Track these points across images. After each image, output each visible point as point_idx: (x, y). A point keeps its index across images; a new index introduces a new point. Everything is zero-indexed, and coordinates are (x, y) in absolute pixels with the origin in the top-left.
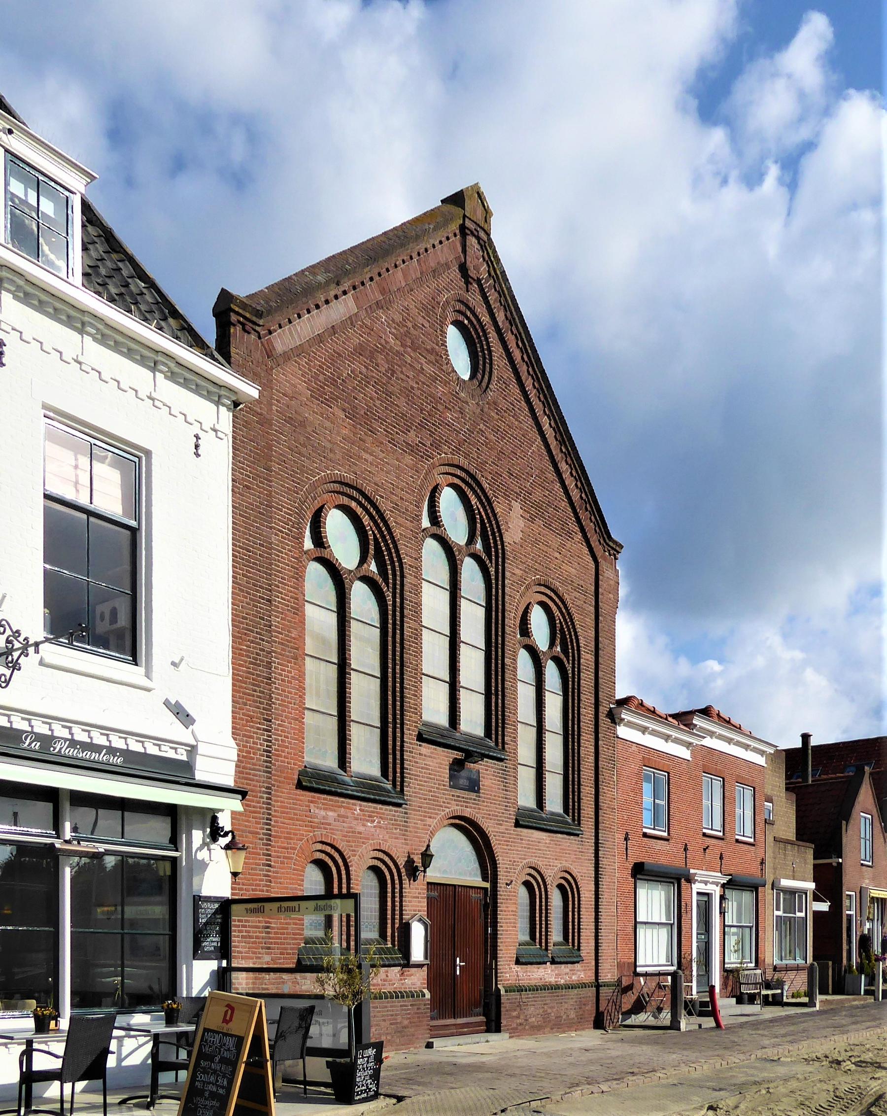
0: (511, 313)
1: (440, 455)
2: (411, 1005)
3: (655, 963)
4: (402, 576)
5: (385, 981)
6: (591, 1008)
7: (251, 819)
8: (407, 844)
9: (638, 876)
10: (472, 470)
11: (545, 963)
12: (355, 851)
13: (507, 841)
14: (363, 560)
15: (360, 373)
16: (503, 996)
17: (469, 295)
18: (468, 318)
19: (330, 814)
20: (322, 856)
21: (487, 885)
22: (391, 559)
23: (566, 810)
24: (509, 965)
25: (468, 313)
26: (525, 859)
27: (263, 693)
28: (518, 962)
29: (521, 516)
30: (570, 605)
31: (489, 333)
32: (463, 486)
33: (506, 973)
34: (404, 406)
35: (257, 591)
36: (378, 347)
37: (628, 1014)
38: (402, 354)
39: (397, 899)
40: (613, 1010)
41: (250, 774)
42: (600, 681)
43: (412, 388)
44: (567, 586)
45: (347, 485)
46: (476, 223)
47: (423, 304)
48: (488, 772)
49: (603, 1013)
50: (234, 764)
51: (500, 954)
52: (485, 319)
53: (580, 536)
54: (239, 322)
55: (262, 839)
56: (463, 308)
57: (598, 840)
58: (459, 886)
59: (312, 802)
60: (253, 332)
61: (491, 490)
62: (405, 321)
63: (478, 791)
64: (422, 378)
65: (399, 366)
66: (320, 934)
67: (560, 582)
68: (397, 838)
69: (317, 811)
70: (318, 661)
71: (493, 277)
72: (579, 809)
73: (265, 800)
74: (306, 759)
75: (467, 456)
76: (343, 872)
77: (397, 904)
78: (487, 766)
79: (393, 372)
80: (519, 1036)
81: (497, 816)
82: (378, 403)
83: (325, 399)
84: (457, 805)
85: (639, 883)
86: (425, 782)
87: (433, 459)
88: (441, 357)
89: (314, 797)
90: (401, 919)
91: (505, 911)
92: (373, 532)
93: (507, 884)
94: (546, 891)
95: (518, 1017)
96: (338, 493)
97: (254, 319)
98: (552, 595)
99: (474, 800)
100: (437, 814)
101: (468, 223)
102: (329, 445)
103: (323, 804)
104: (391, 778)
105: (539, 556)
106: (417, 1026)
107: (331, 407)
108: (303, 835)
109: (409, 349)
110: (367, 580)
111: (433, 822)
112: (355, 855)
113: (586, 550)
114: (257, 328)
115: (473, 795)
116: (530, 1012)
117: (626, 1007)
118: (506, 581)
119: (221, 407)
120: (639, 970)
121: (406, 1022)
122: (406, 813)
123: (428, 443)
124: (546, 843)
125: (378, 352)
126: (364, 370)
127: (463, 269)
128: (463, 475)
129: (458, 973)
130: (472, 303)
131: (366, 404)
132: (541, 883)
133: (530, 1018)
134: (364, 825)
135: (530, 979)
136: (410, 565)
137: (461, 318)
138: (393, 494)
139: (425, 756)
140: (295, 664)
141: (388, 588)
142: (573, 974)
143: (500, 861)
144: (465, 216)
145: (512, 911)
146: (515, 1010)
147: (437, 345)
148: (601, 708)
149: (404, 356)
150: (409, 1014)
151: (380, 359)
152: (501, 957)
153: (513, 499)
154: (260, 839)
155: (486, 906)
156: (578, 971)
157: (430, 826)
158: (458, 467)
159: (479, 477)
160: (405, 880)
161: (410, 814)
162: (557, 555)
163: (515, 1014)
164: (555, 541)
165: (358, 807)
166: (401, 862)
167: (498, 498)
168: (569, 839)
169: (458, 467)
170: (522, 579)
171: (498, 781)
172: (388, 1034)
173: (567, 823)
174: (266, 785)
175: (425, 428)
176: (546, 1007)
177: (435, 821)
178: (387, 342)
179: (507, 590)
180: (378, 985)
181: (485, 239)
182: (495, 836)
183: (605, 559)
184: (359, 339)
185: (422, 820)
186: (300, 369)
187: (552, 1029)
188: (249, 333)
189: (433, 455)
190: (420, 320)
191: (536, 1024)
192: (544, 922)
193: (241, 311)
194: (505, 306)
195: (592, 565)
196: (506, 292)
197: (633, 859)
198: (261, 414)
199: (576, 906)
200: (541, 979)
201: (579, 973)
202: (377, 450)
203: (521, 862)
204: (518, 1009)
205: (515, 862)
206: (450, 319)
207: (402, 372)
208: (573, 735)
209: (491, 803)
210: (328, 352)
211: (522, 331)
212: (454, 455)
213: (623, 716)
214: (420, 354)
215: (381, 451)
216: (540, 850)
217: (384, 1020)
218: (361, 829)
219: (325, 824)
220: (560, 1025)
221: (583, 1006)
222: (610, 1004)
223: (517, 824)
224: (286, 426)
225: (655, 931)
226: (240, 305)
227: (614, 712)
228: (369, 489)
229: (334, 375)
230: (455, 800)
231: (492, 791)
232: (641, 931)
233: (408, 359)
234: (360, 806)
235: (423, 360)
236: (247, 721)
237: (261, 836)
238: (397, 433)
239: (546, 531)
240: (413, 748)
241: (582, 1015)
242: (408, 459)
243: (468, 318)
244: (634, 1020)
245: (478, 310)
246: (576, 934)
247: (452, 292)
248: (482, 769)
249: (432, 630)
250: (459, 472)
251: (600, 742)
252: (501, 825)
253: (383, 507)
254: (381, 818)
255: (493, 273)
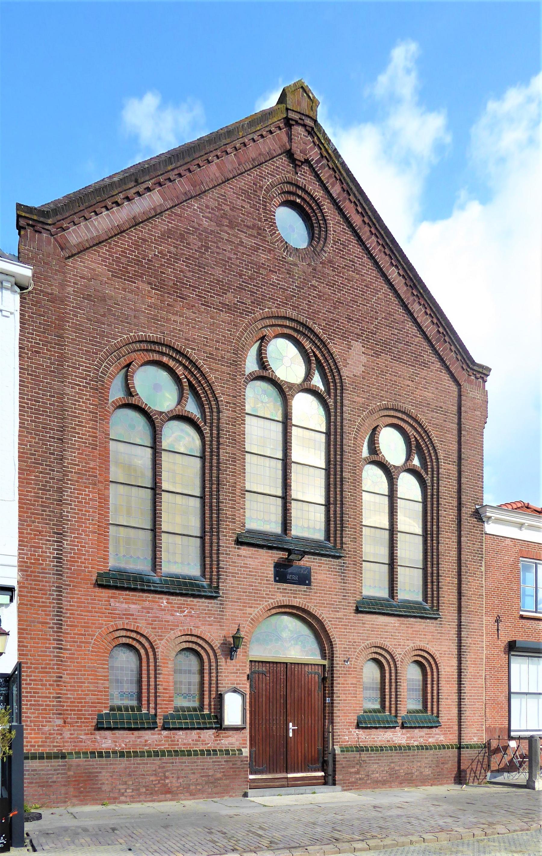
0: (347, 184)
1: (263, 310)
2: (225, 761)
3: (524, 728)
4: (219, 412)
5: (197, 741)
6: (452, 765)
7: (40, 612)
8: (223, 630)
9: (512, 653)
10: (302, 319)
11: (394, 727)
12: (161, 636)
13: (345, 625)
14: (409, 457)
15: (168, 252)
16: (339, 755)
17: (298, 177)
18: (299, 197)
19: (133, 606)
20: (185, 645)
21: (325, 662)
22: (208, 399)
23: (425, 599)
24: (349, 729)
25: (300, 192)
26: (367, 640)
27: (53, 512)
28: (358, 727)
29: (363, 353)
30: (425, 424)
31: (323, 205)
32: (295, 335)
33: (344, 736)
34: (221, 274)
35: (46, 432)
36: (189, 229)
37: (500, 771)
38: (218, 233)
39: (214, 675)
40: (479, 768)
41: (39, 577)
42: (463, 486)
43: (230, 258)
44: (421, 408)
45: (154, 343)
46: (300, 113)
47: (243, 190)
48: (322, 568)
49: (465, 771)
50: (16, 569)
51: (336, 720)
52: (319, 194)
53: (438, 365)
54: (28, 225)
55: (53, 628)
56: (292, 189)
57: (461, 622)
58: (291, 663)
59: (112, 597)
60: (43, 231)
61: (326, 334)
62: (221, 205)
63: (309, 584)
64: (241, 249)
65: (214, 242)
66: (134, 703)
67: (412, 405)
68: (211, 625)
69: (117, 604)
70: (130, 487)
71: (326, 157)
72: (438, 597)
73: (55, 597)
74: (363, 594)
75: (294, 308)
76: (435, 670)
77: (214, 678)
78: (320, 563)
79: (207, 248)
80: (358, 789)
81: (333, 604)
82: (189, 274)
83: (128, 277)
84: (283, 596)
85: (513, 659)
86: (244, 578)
87: (254, 314)
88: (264, 230)
89: (114, 594)
90: (217, 691)
91: (343, 684)
92: (188, 380)
93: (344, 661)
94: (396, 667)
95: (358, 773)
96: (147, 350)
97: (42, 219)
98: (405, 417)
99: (304, 591)
100: (260, 604)
101: (291, 115)
102: (132, 313)
103: (124, 599)
104: (208, 577)
105: (386, 385)
106: (233, 778)
107: (135, 283)
108: (102, 624)
109: (226, 228)
110: (413, 471)
111: (254, 612)
112: (162, 640)
113: (447, 377)
114: (47, 227)
115: (303, 588)
116: (373, 769)
117: (494, 767)
118: (345, 409)
119: (4, 291)
120: (513, 734)
121: (219, 775)
122: (221, 604)
123: (249, 302)
124: (395, 626)
125: (190, 233)
126: (173, 249)
127: (290, 154)
128: (293, 324)
129: (291, 735)
130: (301, 181)
131: (174, 277)
132: (390, 660)
133: (373, 774)
134: (172, 615)
135: (374, 741)
136: (227, 402)
137: (292, 198)
138: (207, 346)
139: (244, 557)
140: (93, 488)
141: (205, 423)
142: (430, 737)
143: (337, 642)
144: (287, 109)
145: (352, 684)
146: (354, 767)
147: (261, 221)
148: (464, 510)
149: (220, 234)
150: (223, 768)
151: (192, 239)
152: (339, 723)
153: (352, 339)
154: (49, 628)
155: (324, 679)
156: (436, 734)
157: (251, 614)
158: (285, 318)
159: (310, 323)
160: (221, 659)
161: (226, 605)
162: (409, 383)
163: (353, 770)
164: (405, 371)
165: (164, 601)
166: (216, 644)
167: (334, 340)
168: (424, 623)
169: (285, 318)
170: (364, 407)
171: (334, 575)
172: (198, 784)
173: (425, 609)
174: (55, 585)
175: (245, 290)
176: (392, 765)
177: (257, 610)
178: (200, 225)
179: (345, 415)
180: (190, 744)
181: (311, 124)
182: (329, 621)
183: (470, 382)
184: (168, 226)
185: (240, 610)
186: (99, 256)
187: (401, 783)
188: (40, 232)
189: (254, 310)
190: (239, 202)
191: (380, 779)
192: (393, 693)
193: (27, 215)
194: (340, 180)
195: (455, 388)
196: (340, 168)
197: (505, 639)
198: (52, 294)
199: (435, 679)
200: (388, 741)
201: (438, 736)
202: (189, 313)
203: (363, 643)
204: (358, 766)
205: (355, 642)
206: (278, 200)
207: (218, 247)
208: (432, 534)
209: (325, 594)
210: (131, 239)
211: (360, 198)
212: (279, 308)
213: (488, 514)
214: (238, 230)
215: (193, 312)
216: (387, 632)
217: (194, 773)
218: (171, 618)
219: (128, 615)
220: (411, 780)
221: (441, 765)
222: (475, 763)
223: (358, 611)
224: (84, 302)
225: (524, 701)
226: (26, 210)
227: (481, 511)
228: (178, 345)
229: (139, 257)
230: (280, 592)
231: (326, 584)
232: (515, 701)
233: (226, 236)
234: (168, 599)
235: (242, 236)
236: (35, 535)
237: (51, 625)
238: (211, 296)
239: (396, 364)
240: (230, 551)
241: (440, 772)
242: (225, 316)
243: (299, 197)
244: (505, 777)
245: (310, 188)
246: (435, 703)
247: (278, 177)
248: (314, 566)
249: (261, 455)
250: (288, 323)
251: (462, 539)
252: (338, 612)
253: (194, 357)
254: (191, 608)
255: (325, 154)
